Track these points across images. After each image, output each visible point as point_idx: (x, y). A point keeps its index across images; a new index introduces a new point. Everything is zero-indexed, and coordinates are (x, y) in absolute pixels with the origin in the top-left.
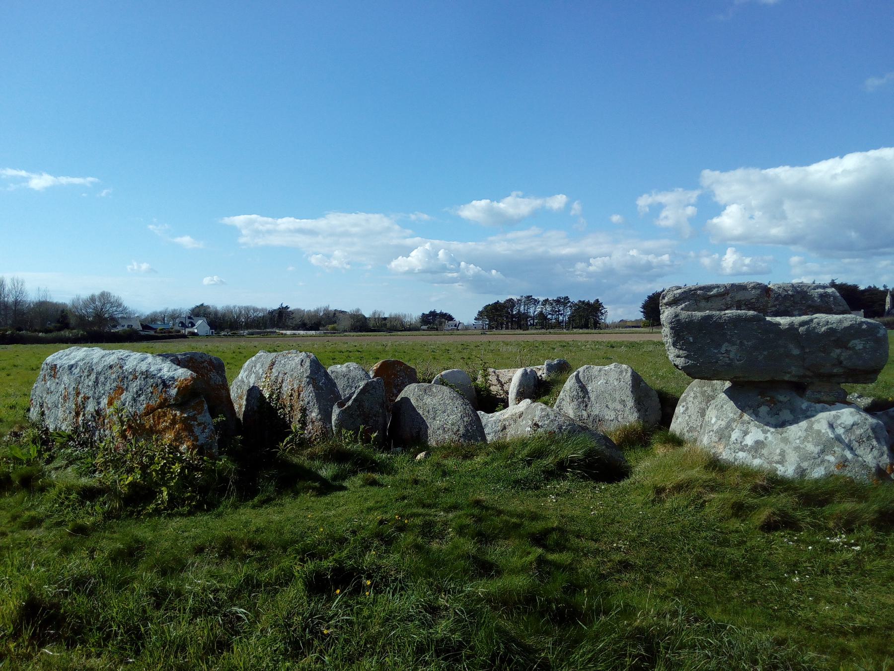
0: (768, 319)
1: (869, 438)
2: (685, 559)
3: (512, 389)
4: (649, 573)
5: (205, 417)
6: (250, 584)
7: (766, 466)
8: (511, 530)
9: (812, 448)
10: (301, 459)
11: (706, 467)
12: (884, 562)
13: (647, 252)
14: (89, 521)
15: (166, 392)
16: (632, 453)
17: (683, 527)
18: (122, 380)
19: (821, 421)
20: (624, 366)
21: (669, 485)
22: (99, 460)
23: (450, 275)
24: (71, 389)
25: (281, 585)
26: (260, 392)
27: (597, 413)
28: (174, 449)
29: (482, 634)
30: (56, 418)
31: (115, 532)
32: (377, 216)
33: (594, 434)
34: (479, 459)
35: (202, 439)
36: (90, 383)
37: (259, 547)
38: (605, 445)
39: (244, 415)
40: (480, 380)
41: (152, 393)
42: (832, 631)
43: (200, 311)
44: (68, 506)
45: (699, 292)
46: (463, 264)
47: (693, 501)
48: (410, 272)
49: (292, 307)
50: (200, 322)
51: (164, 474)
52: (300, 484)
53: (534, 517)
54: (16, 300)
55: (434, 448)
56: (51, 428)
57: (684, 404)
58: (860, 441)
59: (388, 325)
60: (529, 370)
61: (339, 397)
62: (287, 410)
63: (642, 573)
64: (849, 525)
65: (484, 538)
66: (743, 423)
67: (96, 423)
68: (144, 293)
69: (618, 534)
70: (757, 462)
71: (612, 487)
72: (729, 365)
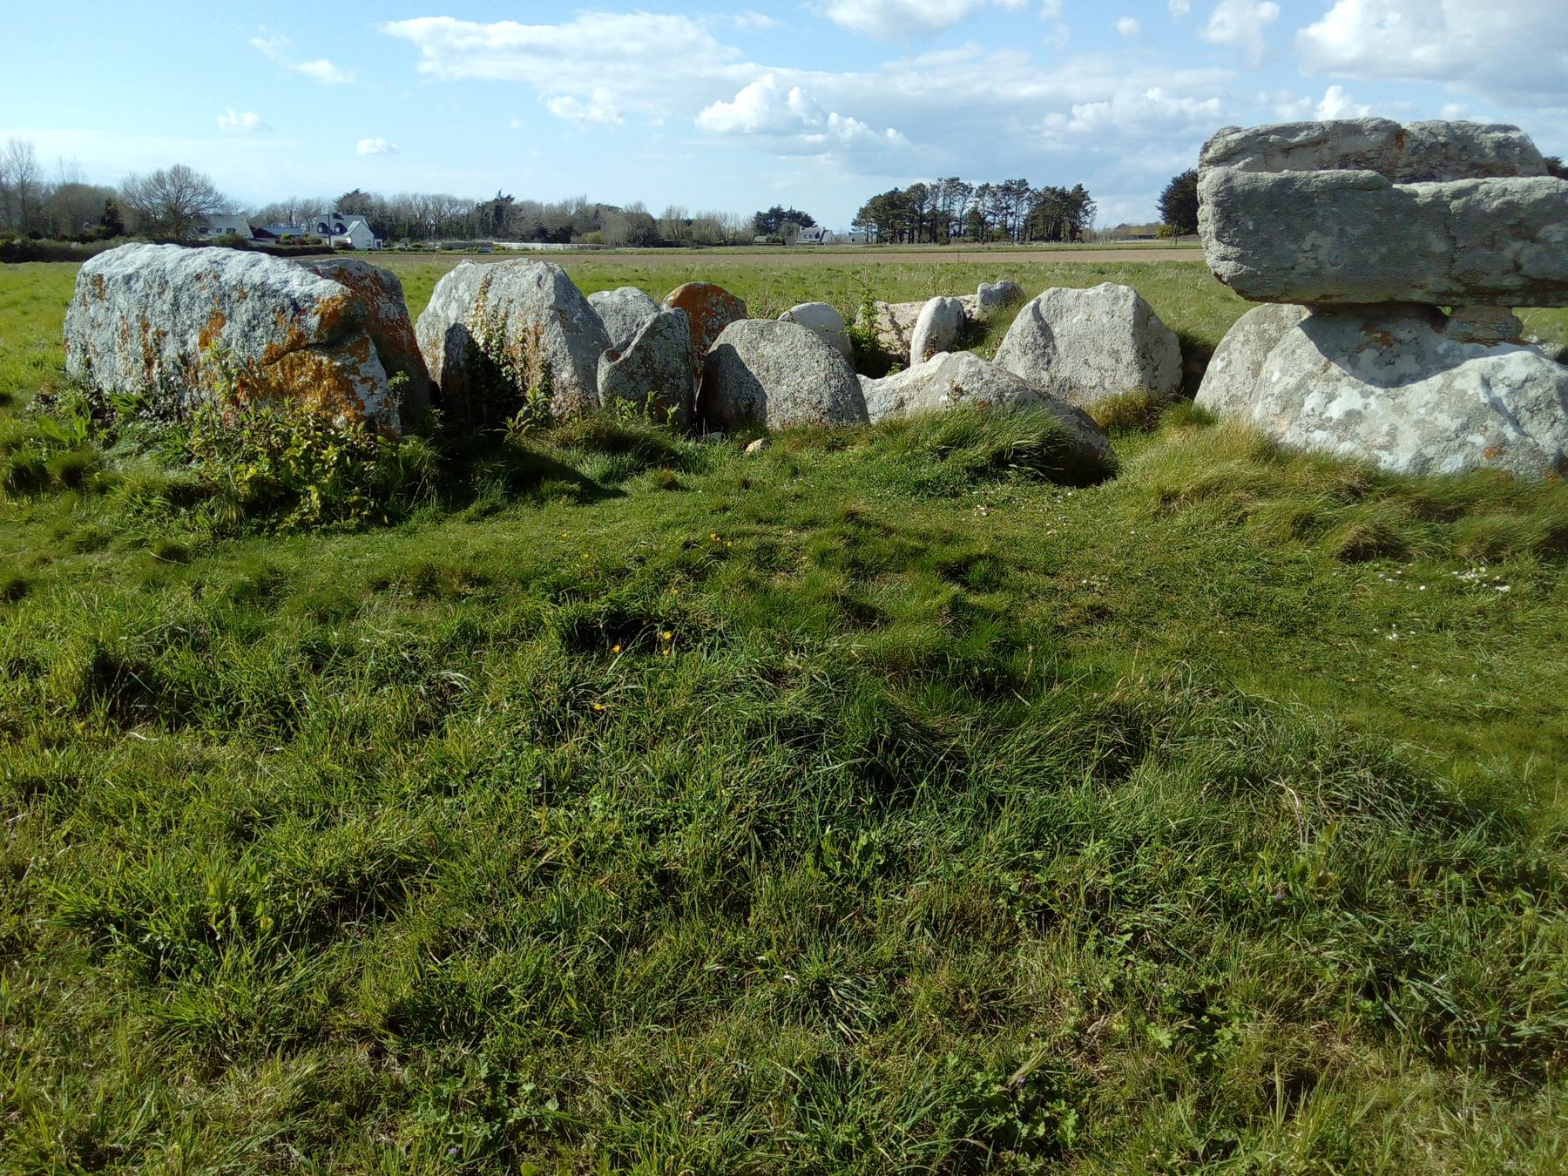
0: (1395, 186)
1: (1550, 404)
2: (1205, 604)
3: (917, 338)
4: (1140, 624)
5: (374, 368)
6: (470, 637)
7: (1362, 454)
8: (907, 558)
9: (1447, 422)
10: (546, 446)
11: (1254, 458)
12: (1548, 611)
13: (1179, 94)
14: (187, 541)
15: (299, 321)
16: (1124, 442)
17: (1205, 554)
18: (221, 302)
19: (1469, 375)
20: (1123, 288)
21: (1186, 487)
22: (196, 441)
23: (810, 138)
24: (133, 318)
25: (522, 638)
26: (468, 334)
27: (1067, 374)
28: (324, 424)
29: (856, 710)
30: (113, 372)
31: (233, 558)
32: (673, 19)
33: (1059, 407)
34: (857, 450)
35: (371, 409)
36: (166, 308)
37: (482, 581)
38: (1079, 424)
39: (443, 375)
40: (860, 323)
41: (275, 323)
42: (1444, 715)
43: (353, 204)
44: (150, 516)
45: (1272, 137)
46: (834, 117)
47: (1227, 513)
48: (736, 132)
49: (520, 198)
50: (355, 224)
51: (310, 464)
52: (546, 486)
53: (949, 539)
54: (23, 182)
55: (778, 435)
56: (107, 388)
57: (1225, 354)
58: (1534, 410)
59: (695, 235)
60: (948, 300)
61: (607, 344)
62: (518, 367)
63: (1127, 625)
64: (1493, 554)
65: (859, 570)
66: (1328, 380)
67: (184, 378)
68: (251, 179)
69: (1092, 565)
70: (1345, 448)
71: (1085, 494)
72: (1314, 274)
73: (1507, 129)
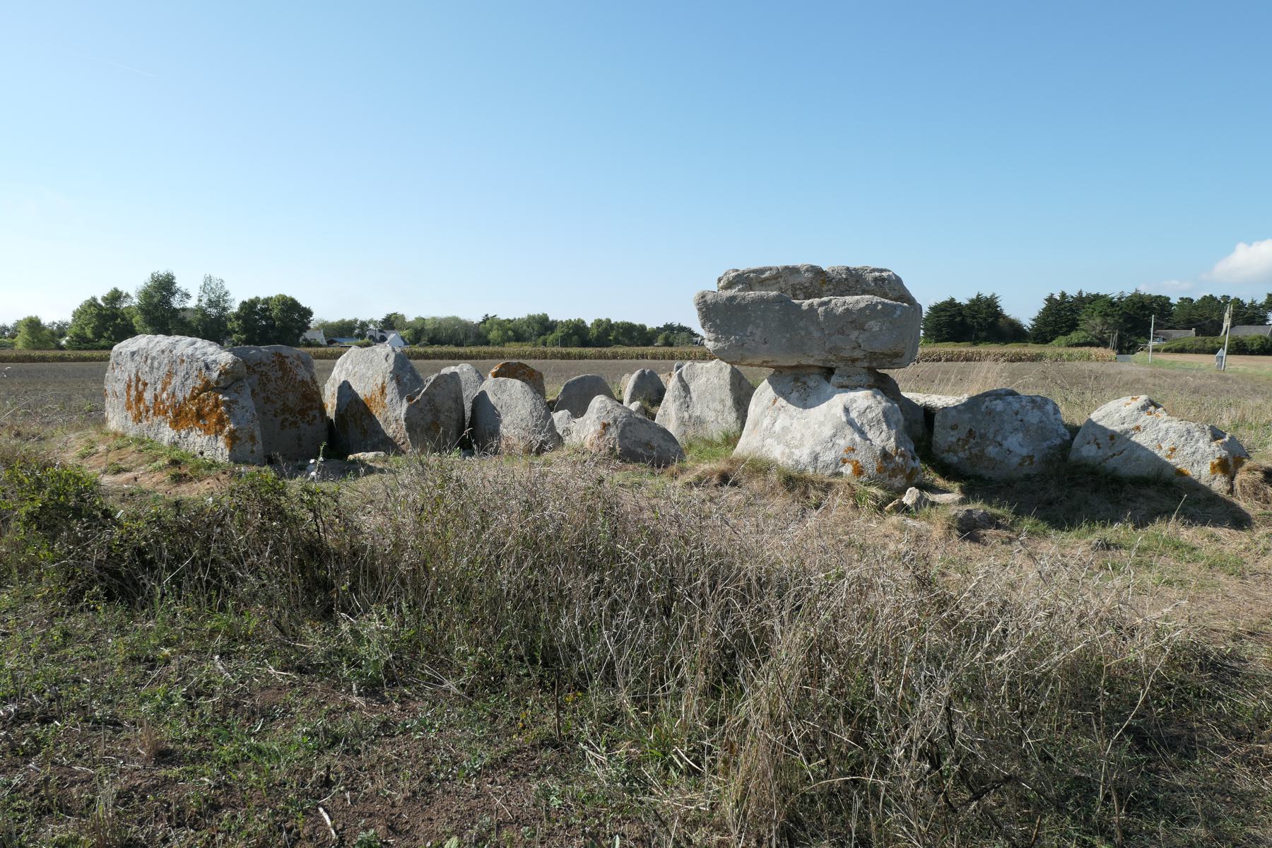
50: (392, 336)
73: (882, 271)
